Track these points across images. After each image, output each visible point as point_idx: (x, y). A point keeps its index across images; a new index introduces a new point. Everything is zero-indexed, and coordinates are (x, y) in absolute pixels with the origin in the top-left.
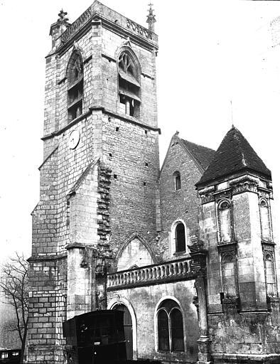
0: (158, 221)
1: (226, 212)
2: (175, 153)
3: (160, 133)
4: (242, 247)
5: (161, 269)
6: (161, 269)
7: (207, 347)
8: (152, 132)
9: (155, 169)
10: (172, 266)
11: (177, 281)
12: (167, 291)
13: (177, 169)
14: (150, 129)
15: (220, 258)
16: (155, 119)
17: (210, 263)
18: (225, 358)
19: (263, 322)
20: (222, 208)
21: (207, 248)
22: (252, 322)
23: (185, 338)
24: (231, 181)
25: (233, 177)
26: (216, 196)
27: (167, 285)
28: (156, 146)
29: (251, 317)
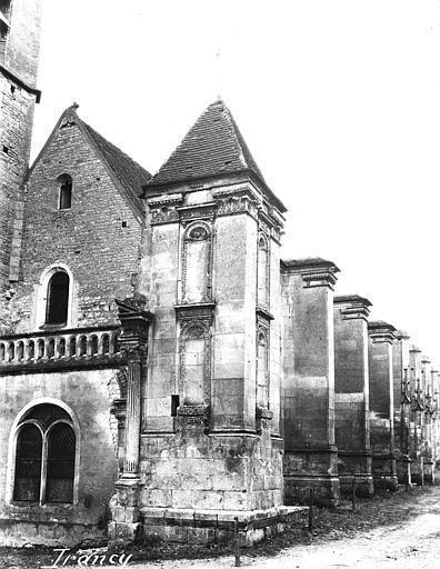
0: (14, 261)
1: (197, 248)
2: (66, 141)
3: (38, 101)
4: (224, 313)
5: (36, 344)
6: (36, 344)
7: (135, 496)
8: (24, 93)
9: (19, 163)
10: (63, 341)
11: (72, 370)
12: (47, 389)
13: (68, 171)
14: (21, 85)
15: (179, 330)
16: (33, 73)
17: (157, 337)
18: (168, 516)
19: (251, 452)
20: (193, 238)
21: (152, 311)
22: (232, 452)
23: (77, 479)
24: (217, 190)
25: (220, 182)
26: (183, 214)
27: (48, 376)
28: (28, 120)
29: (231, 442)
